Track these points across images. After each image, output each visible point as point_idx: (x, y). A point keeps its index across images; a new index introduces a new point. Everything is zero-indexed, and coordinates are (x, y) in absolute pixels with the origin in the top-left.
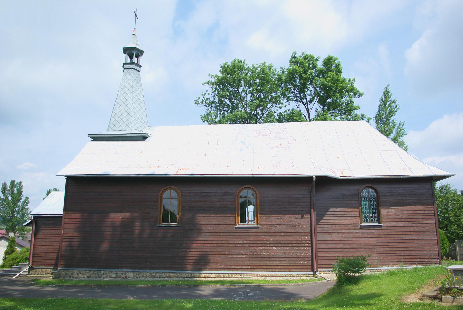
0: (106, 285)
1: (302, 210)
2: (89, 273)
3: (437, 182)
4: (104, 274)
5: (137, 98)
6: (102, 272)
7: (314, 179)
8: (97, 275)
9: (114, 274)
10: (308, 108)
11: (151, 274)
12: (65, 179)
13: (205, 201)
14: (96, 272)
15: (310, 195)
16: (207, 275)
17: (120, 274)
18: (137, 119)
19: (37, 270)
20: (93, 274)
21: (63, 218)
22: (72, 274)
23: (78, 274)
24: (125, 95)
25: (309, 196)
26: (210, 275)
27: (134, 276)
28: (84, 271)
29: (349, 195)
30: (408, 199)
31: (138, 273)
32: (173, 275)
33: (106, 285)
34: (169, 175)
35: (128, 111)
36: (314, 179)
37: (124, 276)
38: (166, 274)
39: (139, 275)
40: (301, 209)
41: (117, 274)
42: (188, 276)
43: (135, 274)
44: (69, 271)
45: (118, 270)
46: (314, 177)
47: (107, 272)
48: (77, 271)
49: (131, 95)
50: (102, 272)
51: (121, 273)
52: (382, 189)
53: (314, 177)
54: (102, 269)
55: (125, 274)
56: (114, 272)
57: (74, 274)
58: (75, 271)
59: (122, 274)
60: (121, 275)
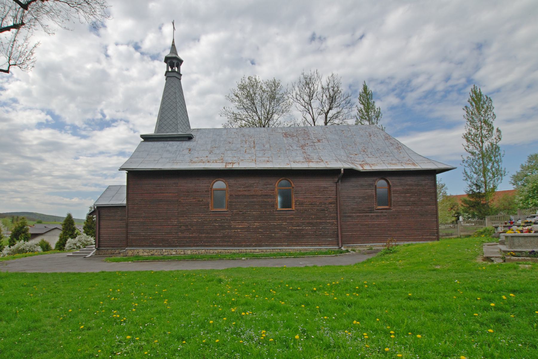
0: (326, 293)
1: (329, 197)
2: (153, 252)
3: (437, 175)
4: (165, 252)
5: (180, 104)
6: (164, 250)
7: (342, 172)
8: (159, 253)
9: (174, 251)
10: (313, 116)
11: (205, 251)
12: (126, 174)
13: (249, 191)
14: (159, 251)
15: (336, 184)
16: (253, 250)
17: (179, 251)
18: (182, 122)
19: (103, 251)
20: (156, 252)
21: (127, 207)
22: (138, 253)
23: (143, 253)
24: (169, 101)
25: (335, 186)
26: (255, 250)
27: (191, 252)
28: (148, 250)
29: (366, 185)
30: (415, 188)
31: (195, 250)
32: (224, 251)
33: (326, 293)
34: (398, 178)
35: (174, 115)
36: (342, 172)
37: (182, 253)
38: (218, 250)
39: (195, 251)
40: (328, 196)
41: (176, 251)
42: (237, 252)
43: (192, 251)
44: (135, 250)
45: (177, 248)
46: (342, 169)
47: (168, 250)
48: (142, 250)
49: (174, 100)
50: (164, 250)
51: (180, 250)
52: (392, 180)
53: (342, 169)
54: (164, 248)
55: (184, 251)
56: (174, 250)
57: (140, 253)
58: (140, 250)
59: (181, 252)
60: (180, 252)
